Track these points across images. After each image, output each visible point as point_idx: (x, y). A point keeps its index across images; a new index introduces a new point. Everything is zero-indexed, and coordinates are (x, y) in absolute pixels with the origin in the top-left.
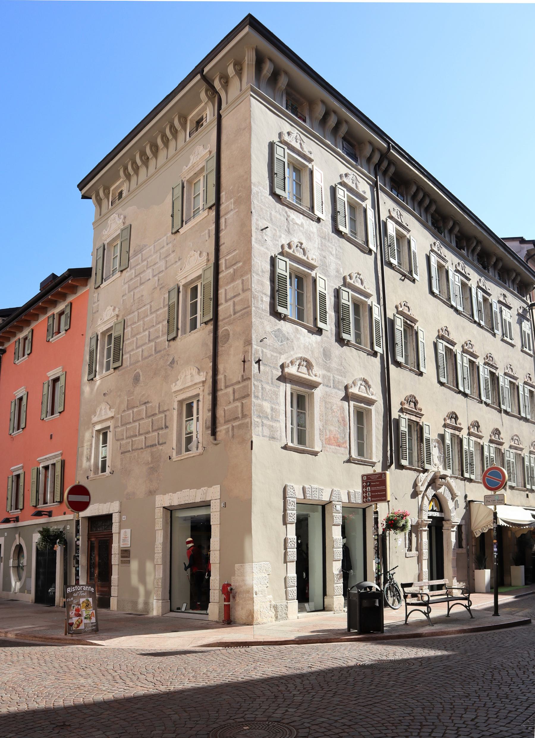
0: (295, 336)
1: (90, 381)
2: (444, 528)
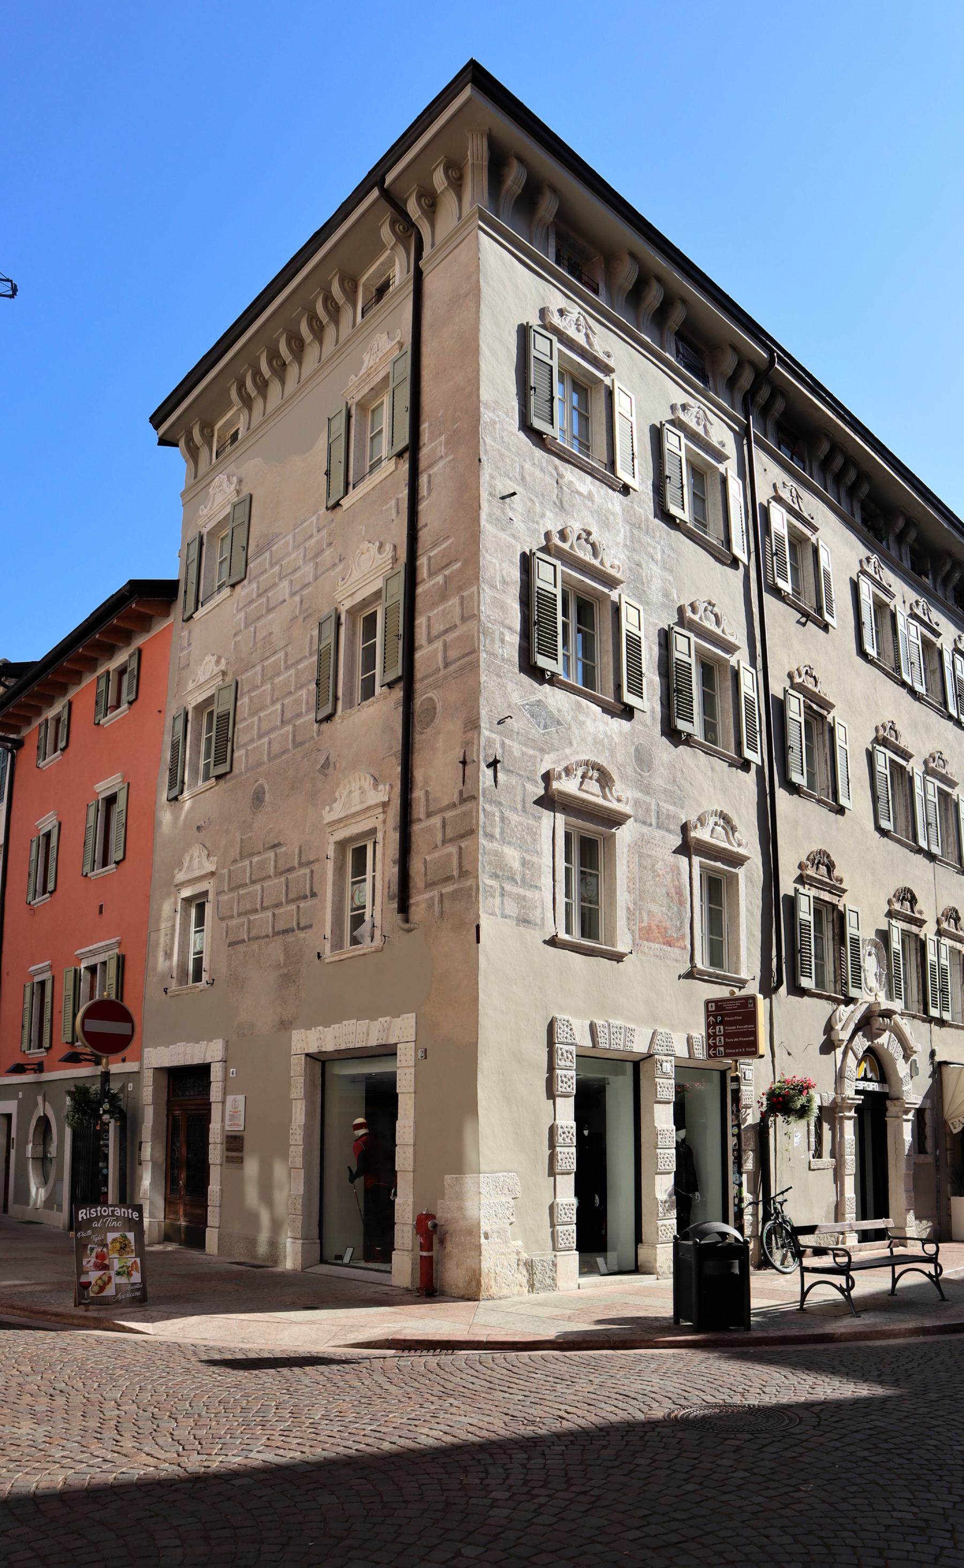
0: (575, 719)
1: (173, 803)
2: (888, 1114)
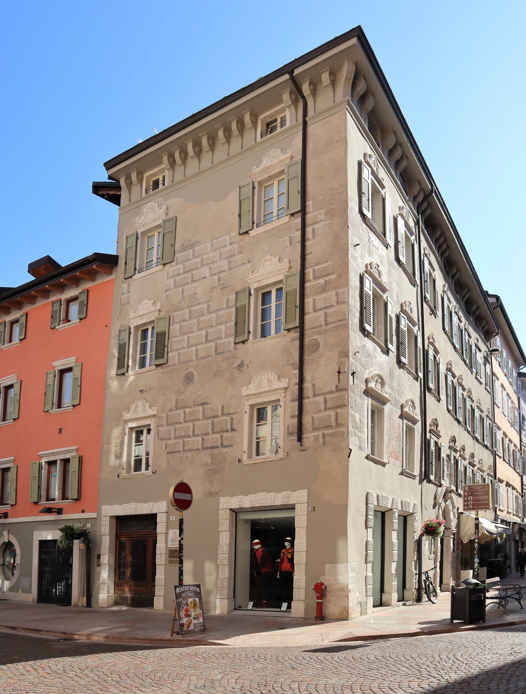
0: (374, 354)
1: (119, 376)
